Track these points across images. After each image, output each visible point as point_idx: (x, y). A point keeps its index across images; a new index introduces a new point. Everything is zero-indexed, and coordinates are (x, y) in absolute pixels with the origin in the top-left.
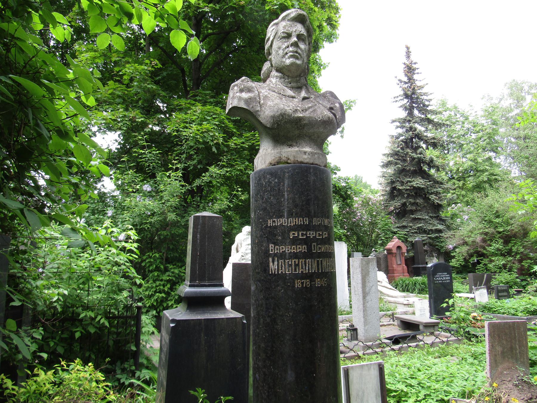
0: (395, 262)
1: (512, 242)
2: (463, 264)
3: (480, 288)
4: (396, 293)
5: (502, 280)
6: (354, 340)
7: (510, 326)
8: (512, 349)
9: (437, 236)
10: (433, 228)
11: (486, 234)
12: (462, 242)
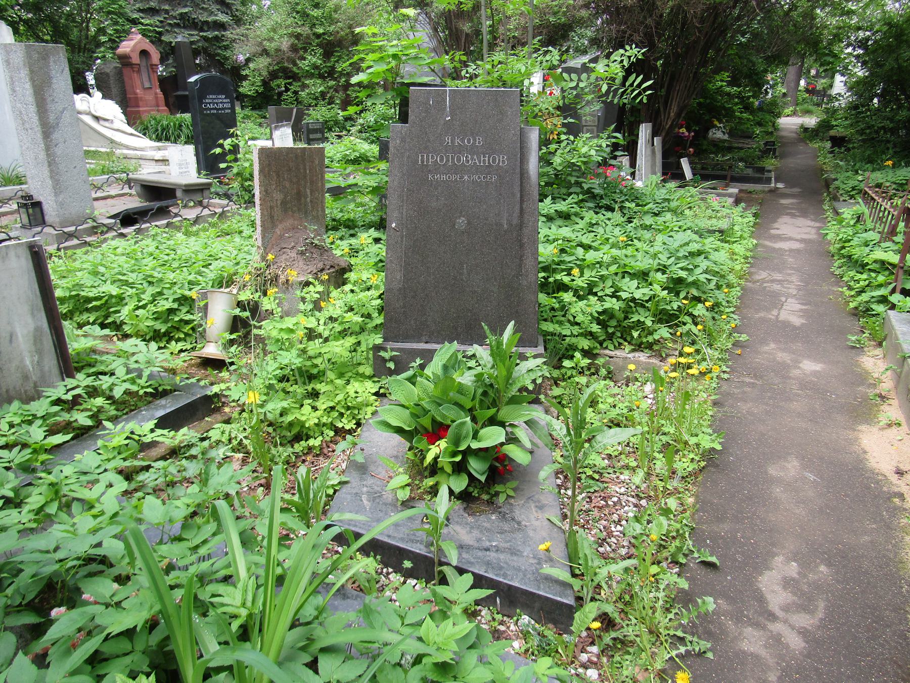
0: (138, 83)
1: (336, 54)
2: (261, 90)
3: (282, 126)
4: (145, 142)
5: (319, 117)
6: (37, 225)
7: (297, 157)
8: (299, 195)
9: (217, 36)
10: (210, 19)
11: (298, 36)
12: (259, 49)
